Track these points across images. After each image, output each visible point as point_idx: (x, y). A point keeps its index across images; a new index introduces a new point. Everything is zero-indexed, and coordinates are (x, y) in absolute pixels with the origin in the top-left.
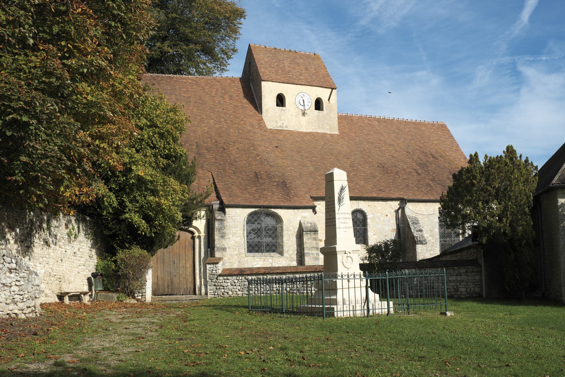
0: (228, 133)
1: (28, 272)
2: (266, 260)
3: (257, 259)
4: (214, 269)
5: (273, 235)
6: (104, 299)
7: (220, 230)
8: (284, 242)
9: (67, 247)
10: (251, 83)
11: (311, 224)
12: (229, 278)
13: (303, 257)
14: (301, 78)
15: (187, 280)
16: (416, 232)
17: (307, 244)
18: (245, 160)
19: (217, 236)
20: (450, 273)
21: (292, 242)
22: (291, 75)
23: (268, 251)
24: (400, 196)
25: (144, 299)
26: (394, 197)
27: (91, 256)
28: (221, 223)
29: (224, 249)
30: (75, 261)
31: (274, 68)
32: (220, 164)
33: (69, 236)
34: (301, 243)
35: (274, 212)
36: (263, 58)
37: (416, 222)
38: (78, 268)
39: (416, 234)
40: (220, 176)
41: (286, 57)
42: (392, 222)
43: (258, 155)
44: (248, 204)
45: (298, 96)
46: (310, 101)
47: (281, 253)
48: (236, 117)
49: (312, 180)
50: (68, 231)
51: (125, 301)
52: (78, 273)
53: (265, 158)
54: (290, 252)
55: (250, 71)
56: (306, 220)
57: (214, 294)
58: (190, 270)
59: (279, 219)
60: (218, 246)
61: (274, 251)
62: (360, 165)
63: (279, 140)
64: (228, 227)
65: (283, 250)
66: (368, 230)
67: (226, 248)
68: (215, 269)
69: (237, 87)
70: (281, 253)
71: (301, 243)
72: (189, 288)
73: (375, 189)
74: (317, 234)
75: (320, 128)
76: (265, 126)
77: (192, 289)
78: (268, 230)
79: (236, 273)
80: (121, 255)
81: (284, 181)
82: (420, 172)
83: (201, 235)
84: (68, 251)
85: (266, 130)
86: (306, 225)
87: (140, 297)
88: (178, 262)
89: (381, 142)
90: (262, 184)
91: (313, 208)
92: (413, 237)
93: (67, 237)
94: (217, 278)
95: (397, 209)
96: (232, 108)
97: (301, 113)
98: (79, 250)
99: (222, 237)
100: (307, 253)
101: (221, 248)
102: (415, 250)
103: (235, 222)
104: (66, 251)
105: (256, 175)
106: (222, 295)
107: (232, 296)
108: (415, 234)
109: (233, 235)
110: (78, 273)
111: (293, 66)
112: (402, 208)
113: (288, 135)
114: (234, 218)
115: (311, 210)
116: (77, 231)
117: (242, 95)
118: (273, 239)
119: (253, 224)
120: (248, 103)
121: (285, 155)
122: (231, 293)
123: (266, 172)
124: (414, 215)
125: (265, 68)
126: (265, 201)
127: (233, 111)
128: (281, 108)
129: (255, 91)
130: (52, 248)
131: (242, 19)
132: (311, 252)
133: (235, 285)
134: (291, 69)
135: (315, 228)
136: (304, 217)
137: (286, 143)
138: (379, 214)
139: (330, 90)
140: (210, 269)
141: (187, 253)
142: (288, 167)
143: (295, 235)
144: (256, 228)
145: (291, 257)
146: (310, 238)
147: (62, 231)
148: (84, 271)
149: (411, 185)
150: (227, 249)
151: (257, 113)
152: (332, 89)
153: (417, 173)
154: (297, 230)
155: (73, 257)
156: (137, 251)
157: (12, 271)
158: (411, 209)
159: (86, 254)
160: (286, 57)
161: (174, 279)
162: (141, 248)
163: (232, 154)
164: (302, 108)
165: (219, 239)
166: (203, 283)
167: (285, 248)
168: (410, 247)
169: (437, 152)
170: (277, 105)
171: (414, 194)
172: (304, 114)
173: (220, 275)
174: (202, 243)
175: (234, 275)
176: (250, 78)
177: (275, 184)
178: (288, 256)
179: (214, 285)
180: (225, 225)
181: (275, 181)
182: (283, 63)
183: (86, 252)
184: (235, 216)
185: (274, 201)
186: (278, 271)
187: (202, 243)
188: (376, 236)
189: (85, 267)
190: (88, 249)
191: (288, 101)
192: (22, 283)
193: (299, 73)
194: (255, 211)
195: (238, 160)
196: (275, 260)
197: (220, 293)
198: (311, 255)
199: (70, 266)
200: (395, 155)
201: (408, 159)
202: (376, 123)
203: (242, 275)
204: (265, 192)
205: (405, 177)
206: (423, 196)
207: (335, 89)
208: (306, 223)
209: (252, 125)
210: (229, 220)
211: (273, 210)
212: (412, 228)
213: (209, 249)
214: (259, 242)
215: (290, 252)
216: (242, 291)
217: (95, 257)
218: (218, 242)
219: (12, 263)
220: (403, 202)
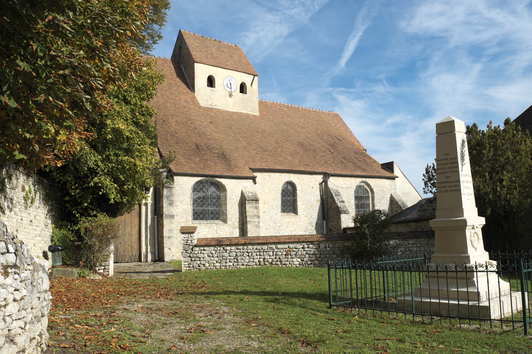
0: (166, 107)
1: (31, 268)
2: (211, 227)
3: (203, 227)
4: (189, 239)
5: (217, 204)
6: (62, 275)
7: (168, 197)
8: (228, 210)
9: (24, 214)
10: (182, 65)
11: (252, 193)
12: (206, 248)
13: (245, 224)
14: (228, 63)
15: (132, 247)
16: (339, 203)
17: (249, 212)
18: (185, 132)
19: (166, 203)
20: (432, 244)
21: (234, 210)
22: (219, 61)
23: (212, 219)
24: (323, 171)
25: (107, 273)
26: (318, 171)
27: (47, 224)
28: (170, 190)
29: (172, 217)
30: (31, 232)
31: (203, 52)
32: (162, 135)
33: (25, 200)
34: (242, 212)
35: (218, 182)
36: (194, 44)
37: (338, 194)
38: (34, 239)
39: (339, 205)
40: (164, 146)
41: (213, 45)
42: (317, 193)
43: (196, 128)
44: (195, 173)
45: (226, 79)
46: (236, 85)
47: (225, 221)
48: (172, 94)
49: (247, 153)
50: (24, 194)
51: (88, 278)
52: (34, 245)
53: (203, 132)
54: (233, 220)
55: (180, 54)
56: (248, 190)
57: (189, 267)
58: (135, 237)
59: (221, 188)
60: (166, 213)
61: (217, 219)
62: (284, 143)
63: (212, 117)
64: (176, 195)
65: (227, 218)
66: (298, 200)
67: (174, 216)
68: (190, 238)
69: (169, 67)
70: (225, 221)
71: (242, 212)
72: (134, 256)
73: (302, 164)
74: (258, 203)
75: (244, 109)
76: (198, 104)
77: (137, 256)
78: (213, 198)
79: (214, 243)
80: (84, 224)
81: (223, 153)
82: (332, 151)
83: (148, 202)
84: (24, 219)
85: (200, 107)
86: (247, 195)
87: (102, 271)
88: (124, 229)
89: (294, 125)
90: (205, 155)
91: (254, 179)
92: (338, 208)
93: (23, 201)
94: (192, 249)
95: (321, 182)
96: (167, 85)
97: (228, 95)
98: (35, 217)
99: (171, 204)
100: (249, 221)
101: (169, 215)
102: (339, 218)
103: (182, 190)
104: (22, 219)
105: (197, 146)
106: (198, 267)
107: (209, 268)
108: (339, 205)
109: (181, 203)
110: (34, 245)
111: (219, 53)
112: (325, 181)
113: (218, 113)
114: (182, 186)
115: (252, 181)
116: (34, 194)
117: (175, 75)
118: (217, 207)
119: (198, 192)
120: (181, 82)
121: (220, 130)
122: (208, 266)
123: (206, 144)
124: (335, 188)
125: (197, 52)
126: (210, 171)
127: (168, 88)
128: (211, 88)
129: (186, 72)
130: (7, 216)
131: (167, 11)
132: (252, 220)
133: (213, 256)
134: (218, 55)
135: (256, 197)
136: (245, 187)
137: (218, 120)
138: (306, 186)
139: (253, 76)
140: (184, 239)
141: (133, 220)
142: (224, 141)
143: (238, 203)
144: (201, 196)
145: (233, 224)
146: (252, 207)
147: (18, 194)
148: (40, 243)
149: (329, 162)
150: (258, 220)
151: (190, 92)
152: (254, 76)
153: (330, 151)
154: (239, 199)
155: (29, 227)
156: (103, 219)
157: (9, 270)
158: (334, 183)
159: (42, 222)
160: (213, 45)
161: (119, 246)
162: (108, 216)
163: (171, 126)
164: (229, 90)
165: (167, 207)
166: (149, 250)
167: (229, 216)
168: (334, 216)
169: (340, 136)
170: (208, 86)
171: (334, 169)
172: (230, 95)
173: (196, 246)
174: (149, 210)
175: (212, 246)
176: (181, 60)
177: (216, 155)
178: (231, 224)
179: (189, 257)
180: (174, 193)
181: (215, 153)
182: (211, 50)
183: (42, 220)
184: (183, 184)
185: (218, 171)
186: (259, 241)
187: (149, 210)
188: (303, 206)
189: (41, 238)
190: (44, 216)
191: (217, 82)
192: (24, 292)
193: (225, 60)
194: (202, 180)
195: (178, 132)
196: (219, 228)
197: (195, 265)
198: (253, 223)
199: (27, 237)
200: (308, 136)
201: (320, 140)
202: (286, 109)
203: (220, 245)
204: (208, 162)
205: (322, 154)
206: (341, 172)
207: (257, 76)
208: (248, 193)
209: (186, 102)
210: (177, 188)
211: (217, 179)
212: (336, 199)
213: (156, 217)
214: (204, 210)
215: (233, 220)
216: (220, 263)
217: (51, 226)
218: (166, 210)
219: (8, 252)
220: (326, 176)
